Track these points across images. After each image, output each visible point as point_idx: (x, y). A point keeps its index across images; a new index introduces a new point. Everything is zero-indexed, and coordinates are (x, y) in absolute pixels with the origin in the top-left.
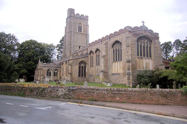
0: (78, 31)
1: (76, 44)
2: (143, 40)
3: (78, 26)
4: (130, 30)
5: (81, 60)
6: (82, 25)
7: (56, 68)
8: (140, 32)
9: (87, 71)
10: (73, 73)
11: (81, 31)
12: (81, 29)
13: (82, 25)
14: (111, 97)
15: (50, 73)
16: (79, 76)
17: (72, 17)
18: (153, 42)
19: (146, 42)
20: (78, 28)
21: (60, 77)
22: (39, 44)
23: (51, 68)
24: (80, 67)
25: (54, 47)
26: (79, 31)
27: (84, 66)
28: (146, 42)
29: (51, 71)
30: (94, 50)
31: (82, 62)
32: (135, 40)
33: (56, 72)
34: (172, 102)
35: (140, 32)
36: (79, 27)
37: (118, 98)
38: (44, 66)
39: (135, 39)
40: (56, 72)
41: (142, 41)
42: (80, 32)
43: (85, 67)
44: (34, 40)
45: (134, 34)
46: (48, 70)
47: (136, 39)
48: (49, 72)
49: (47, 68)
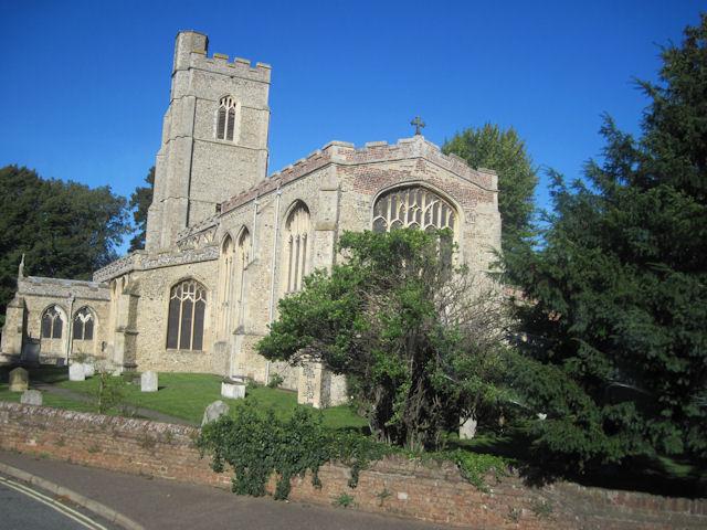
0: (215, 135)
1: (205, 196)
2: (410, 203)
3: (216, 113)
4: (344, 158)
5: (181, 273)
6: (239, 105)
7: (53, 300)
8: (394, 166)
9: (207, 324)
10: (140, 329)
11: (230, 136)
12: (231, 127)
13: (238, 110)
14: (17, 435)
15: (59, 323)
16: (170, 344)
17: (192, 71)
18: (459, 207)
19: (424, 210)
20: (216, 120)
21: (104, 345)
22: (52, 188)
23: (62, 300)
24: (173, 305)
25: (121, 202)
26: (221, 137)
27: (194, 301)
28: (424, 210)
29: (63, 317)
30: (236, 233)
31: (186, 282)
32: (363, 203)
33: (84, 320)
34: (163, 469)
35: (394, 166)
36: (222, 112)
37: (33, 442)
38: (32, 292)
39: (366, 198)
40: (84, 320)
41: (407, 207)
42: (225, 141)
43: (201, 307)
44: (24, 169)
45: (362, 177)
46: (52, 308)
47: (369, 198)
48: (53, 318)
49: (45, 303)
